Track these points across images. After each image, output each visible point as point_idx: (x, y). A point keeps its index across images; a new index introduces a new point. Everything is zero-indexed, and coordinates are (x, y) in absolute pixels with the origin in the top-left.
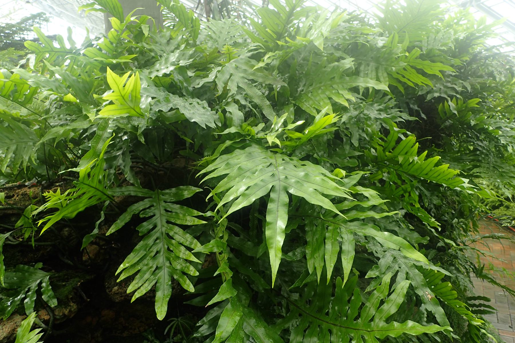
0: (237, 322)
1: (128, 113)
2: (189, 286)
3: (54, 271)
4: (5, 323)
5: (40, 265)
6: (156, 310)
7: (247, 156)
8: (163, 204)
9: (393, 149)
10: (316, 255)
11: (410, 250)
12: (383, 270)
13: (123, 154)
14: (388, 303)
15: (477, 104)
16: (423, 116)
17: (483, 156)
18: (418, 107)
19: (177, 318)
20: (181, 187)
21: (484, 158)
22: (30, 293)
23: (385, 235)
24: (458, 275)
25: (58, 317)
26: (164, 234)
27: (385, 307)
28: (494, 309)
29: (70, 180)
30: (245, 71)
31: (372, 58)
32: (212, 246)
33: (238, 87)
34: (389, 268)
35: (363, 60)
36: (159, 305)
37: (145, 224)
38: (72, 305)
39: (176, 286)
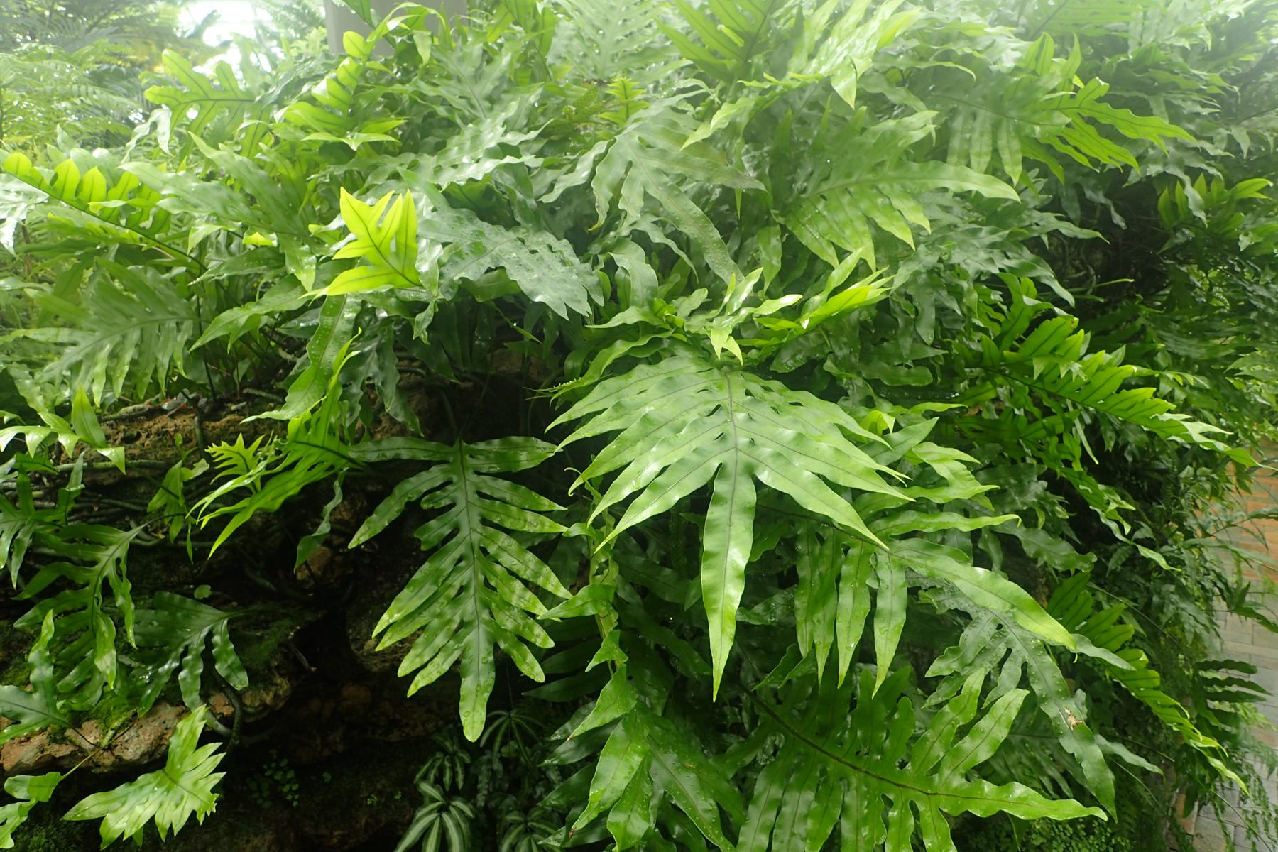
0: (636, 768)
1: (390, 283)
2: (532, 668)
3: (235, 604)
4: (143, 722)
5: (205, 591)
6: (463, 719)
7: (663, 384)
8: (474, 478)
9: (1020, 341)
10: (819, 615)
11: (1034, 615)
12: (970, 656)
13: (379, 350)
14: (973, 738)
15: (1261, 191)
16: (1118, 219)
17: (1266, 324)
18: (1106, 196)
19: (509, 710)
20: (514, 438)
21: (1267, 329)
22: (189, 657)
23: (979, 575)
24: (1183, 605)
25: (250, 710)
26: (476, 548)
27: (967, 743)
28: (1262, 691)
29: (260, 397)
30: (663, 154)
31: (984, 97)
32: (581, 603)
33: (647, 197)
34: (984, 651)
35: (960, 101)
36: (469, 708)
37: (433, 523)
38: (279, 681)
39: (505, 667)
